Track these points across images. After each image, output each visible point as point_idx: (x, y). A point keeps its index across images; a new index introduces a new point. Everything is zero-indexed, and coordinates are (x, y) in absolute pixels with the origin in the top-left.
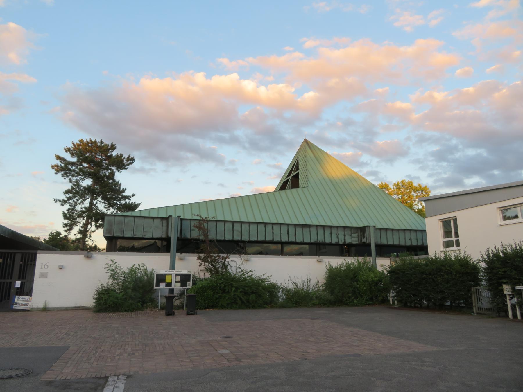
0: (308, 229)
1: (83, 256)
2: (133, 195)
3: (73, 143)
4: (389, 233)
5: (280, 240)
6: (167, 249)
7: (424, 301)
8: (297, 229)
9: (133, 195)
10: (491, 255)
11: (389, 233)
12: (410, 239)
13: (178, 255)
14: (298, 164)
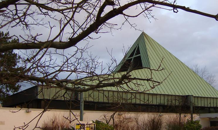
0: (155, 97)
1: (25, 111)
2: (61, 18)
3: (48, 117)
4: (199, 99)
5: (139, 103)
6: (77, 108)
7: (16, 85)
8: (149, 96)
9: (61, 18)
10: (36, 89)
11: (199, 99)
12: (210, 103)
13: (84, 111)
14: (138, 46)
